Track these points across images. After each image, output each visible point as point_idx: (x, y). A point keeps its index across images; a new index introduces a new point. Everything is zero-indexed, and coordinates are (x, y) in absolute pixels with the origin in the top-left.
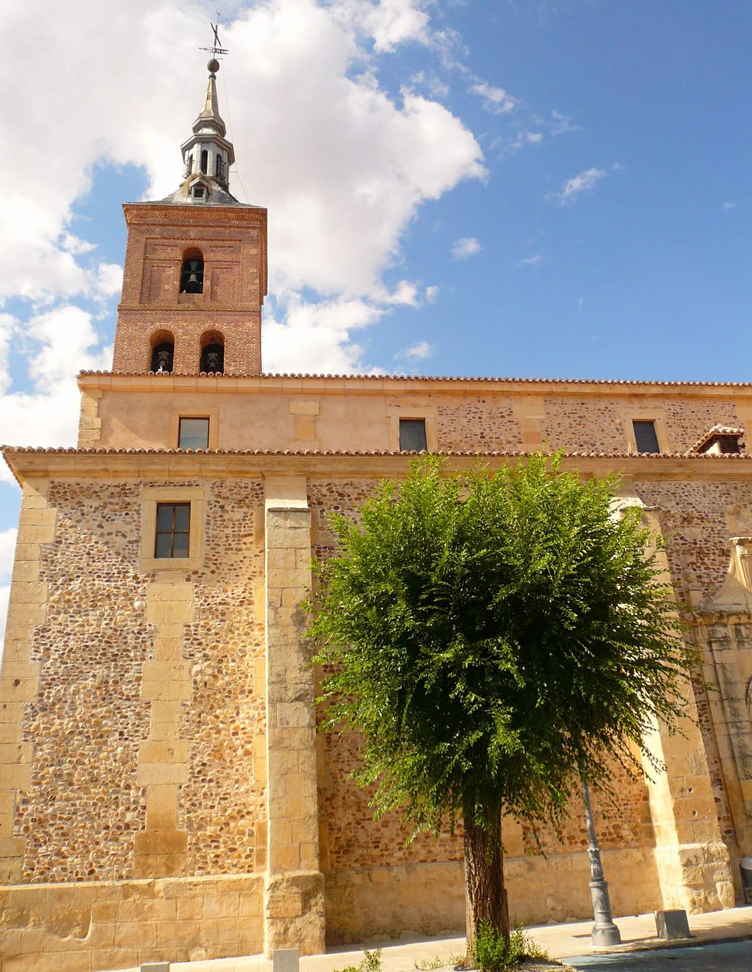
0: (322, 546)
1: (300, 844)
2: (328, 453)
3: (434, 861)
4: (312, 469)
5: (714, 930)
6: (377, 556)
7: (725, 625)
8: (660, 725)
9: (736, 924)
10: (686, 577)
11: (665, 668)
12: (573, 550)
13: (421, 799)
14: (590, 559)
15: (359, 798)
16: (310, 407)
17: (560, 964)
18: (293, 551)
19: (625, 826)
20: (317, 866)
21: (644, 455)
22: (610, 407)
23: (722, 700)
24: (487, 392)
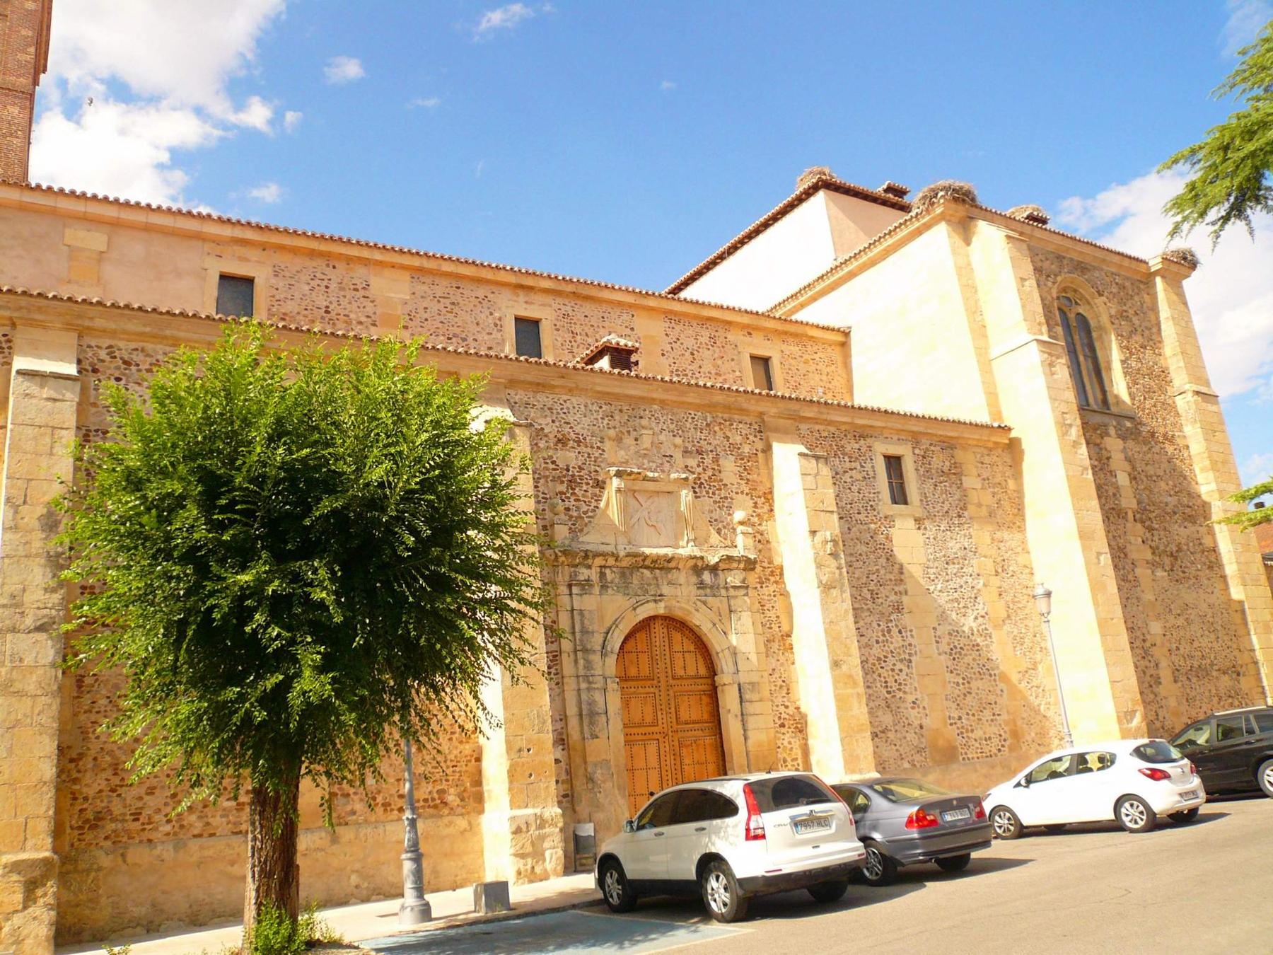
0: (92, 428)
1: (26, 819)
2: (113, 305)
3: (213, 835)
4: (87, 323)
5: (536, 901)
6: (164, 444)
7: (589, 567)
8: (503, 675)
9: (562, 894)
10: (553, 506)
11: (513, 610)
12: (419, 460)
13: (197, 758)
14: (437, 472)
15: (118, 759)
16: (96, 240)
17: (357, 948)
18: (49, 431)
19: (452, 790)
20: (50, 846)
21: (522, 358)
22: (491, 296)
23: (575, 651)
24: (340, 257)
